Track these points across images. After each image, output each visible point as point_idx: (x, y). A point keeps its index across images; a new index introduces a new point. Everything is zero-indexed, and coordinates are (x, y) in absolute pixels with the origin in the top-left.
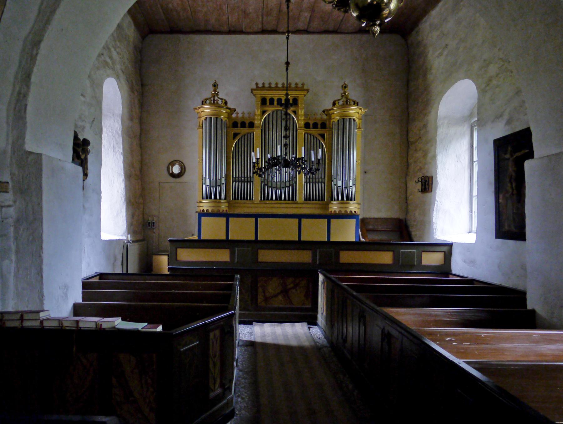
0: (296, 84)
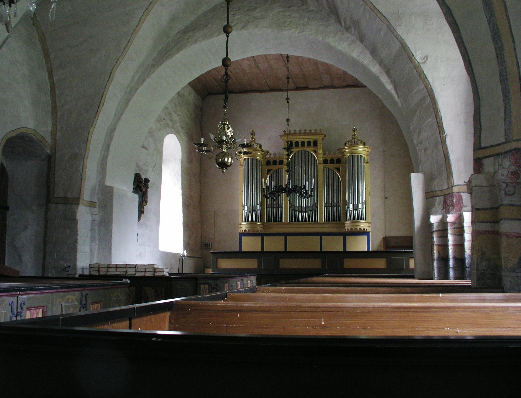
0: (316, 130)
